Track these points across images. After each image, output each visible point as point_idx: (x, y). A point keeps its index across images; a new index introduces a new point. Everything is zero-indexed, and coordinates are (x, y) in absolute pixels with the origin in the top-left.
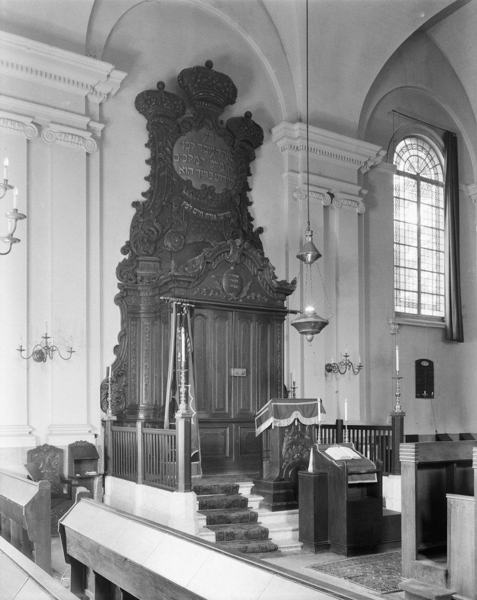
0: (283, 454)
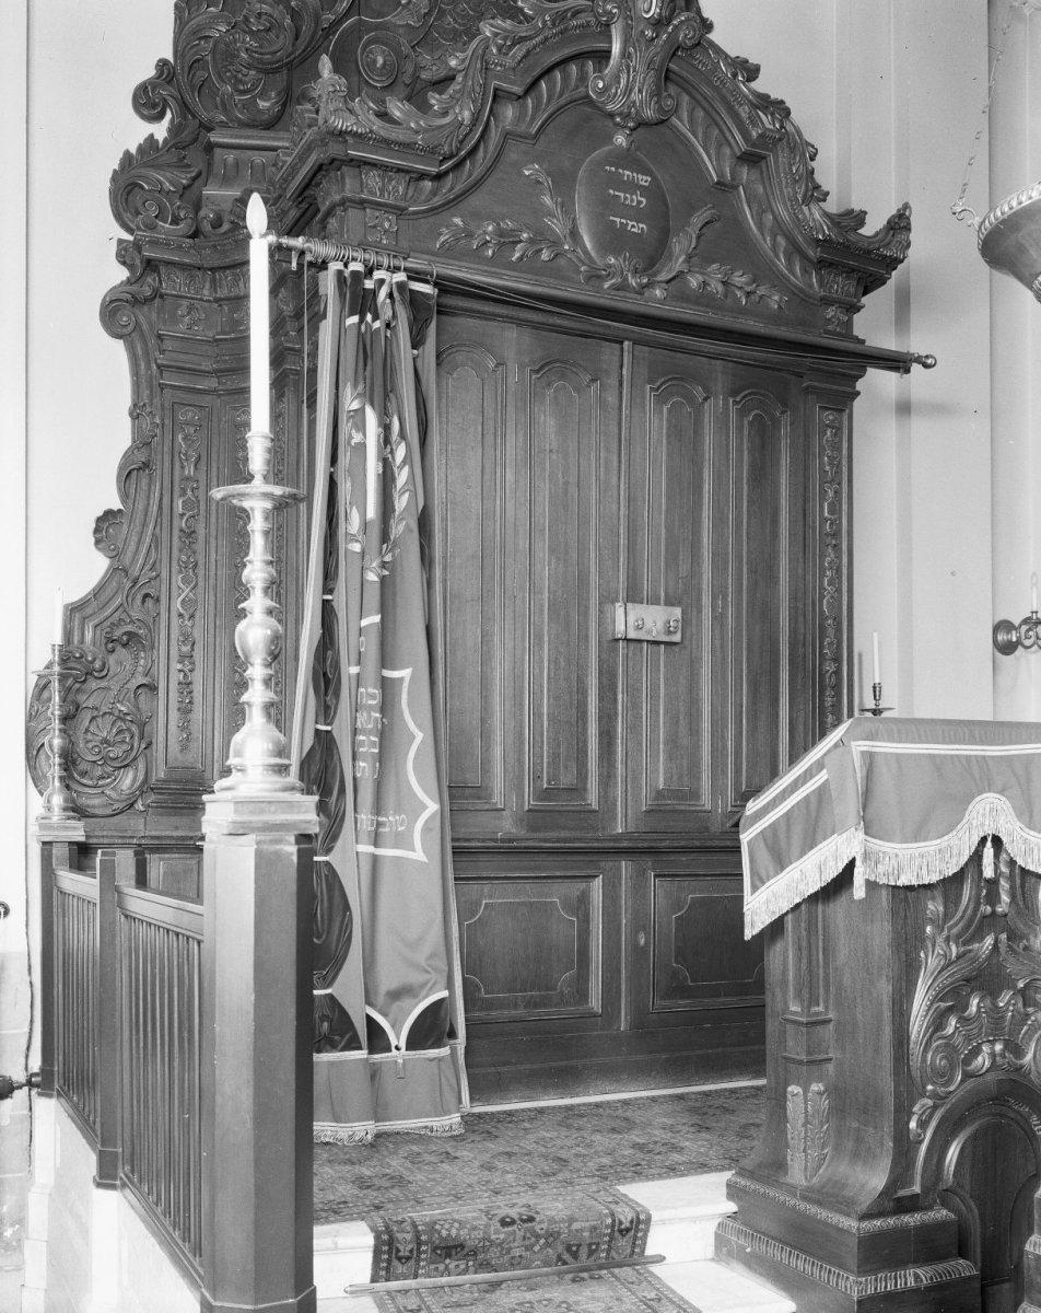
0: (916, 1049)
